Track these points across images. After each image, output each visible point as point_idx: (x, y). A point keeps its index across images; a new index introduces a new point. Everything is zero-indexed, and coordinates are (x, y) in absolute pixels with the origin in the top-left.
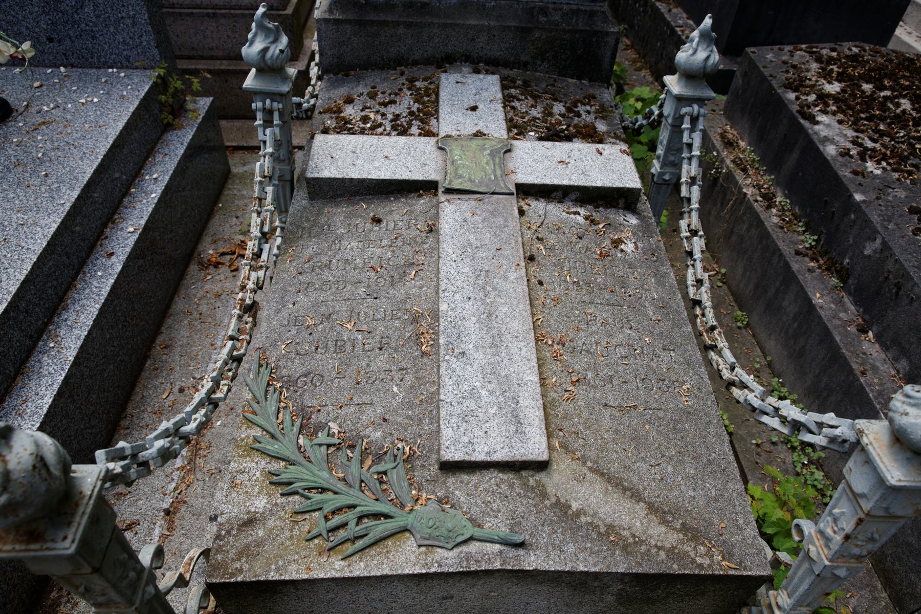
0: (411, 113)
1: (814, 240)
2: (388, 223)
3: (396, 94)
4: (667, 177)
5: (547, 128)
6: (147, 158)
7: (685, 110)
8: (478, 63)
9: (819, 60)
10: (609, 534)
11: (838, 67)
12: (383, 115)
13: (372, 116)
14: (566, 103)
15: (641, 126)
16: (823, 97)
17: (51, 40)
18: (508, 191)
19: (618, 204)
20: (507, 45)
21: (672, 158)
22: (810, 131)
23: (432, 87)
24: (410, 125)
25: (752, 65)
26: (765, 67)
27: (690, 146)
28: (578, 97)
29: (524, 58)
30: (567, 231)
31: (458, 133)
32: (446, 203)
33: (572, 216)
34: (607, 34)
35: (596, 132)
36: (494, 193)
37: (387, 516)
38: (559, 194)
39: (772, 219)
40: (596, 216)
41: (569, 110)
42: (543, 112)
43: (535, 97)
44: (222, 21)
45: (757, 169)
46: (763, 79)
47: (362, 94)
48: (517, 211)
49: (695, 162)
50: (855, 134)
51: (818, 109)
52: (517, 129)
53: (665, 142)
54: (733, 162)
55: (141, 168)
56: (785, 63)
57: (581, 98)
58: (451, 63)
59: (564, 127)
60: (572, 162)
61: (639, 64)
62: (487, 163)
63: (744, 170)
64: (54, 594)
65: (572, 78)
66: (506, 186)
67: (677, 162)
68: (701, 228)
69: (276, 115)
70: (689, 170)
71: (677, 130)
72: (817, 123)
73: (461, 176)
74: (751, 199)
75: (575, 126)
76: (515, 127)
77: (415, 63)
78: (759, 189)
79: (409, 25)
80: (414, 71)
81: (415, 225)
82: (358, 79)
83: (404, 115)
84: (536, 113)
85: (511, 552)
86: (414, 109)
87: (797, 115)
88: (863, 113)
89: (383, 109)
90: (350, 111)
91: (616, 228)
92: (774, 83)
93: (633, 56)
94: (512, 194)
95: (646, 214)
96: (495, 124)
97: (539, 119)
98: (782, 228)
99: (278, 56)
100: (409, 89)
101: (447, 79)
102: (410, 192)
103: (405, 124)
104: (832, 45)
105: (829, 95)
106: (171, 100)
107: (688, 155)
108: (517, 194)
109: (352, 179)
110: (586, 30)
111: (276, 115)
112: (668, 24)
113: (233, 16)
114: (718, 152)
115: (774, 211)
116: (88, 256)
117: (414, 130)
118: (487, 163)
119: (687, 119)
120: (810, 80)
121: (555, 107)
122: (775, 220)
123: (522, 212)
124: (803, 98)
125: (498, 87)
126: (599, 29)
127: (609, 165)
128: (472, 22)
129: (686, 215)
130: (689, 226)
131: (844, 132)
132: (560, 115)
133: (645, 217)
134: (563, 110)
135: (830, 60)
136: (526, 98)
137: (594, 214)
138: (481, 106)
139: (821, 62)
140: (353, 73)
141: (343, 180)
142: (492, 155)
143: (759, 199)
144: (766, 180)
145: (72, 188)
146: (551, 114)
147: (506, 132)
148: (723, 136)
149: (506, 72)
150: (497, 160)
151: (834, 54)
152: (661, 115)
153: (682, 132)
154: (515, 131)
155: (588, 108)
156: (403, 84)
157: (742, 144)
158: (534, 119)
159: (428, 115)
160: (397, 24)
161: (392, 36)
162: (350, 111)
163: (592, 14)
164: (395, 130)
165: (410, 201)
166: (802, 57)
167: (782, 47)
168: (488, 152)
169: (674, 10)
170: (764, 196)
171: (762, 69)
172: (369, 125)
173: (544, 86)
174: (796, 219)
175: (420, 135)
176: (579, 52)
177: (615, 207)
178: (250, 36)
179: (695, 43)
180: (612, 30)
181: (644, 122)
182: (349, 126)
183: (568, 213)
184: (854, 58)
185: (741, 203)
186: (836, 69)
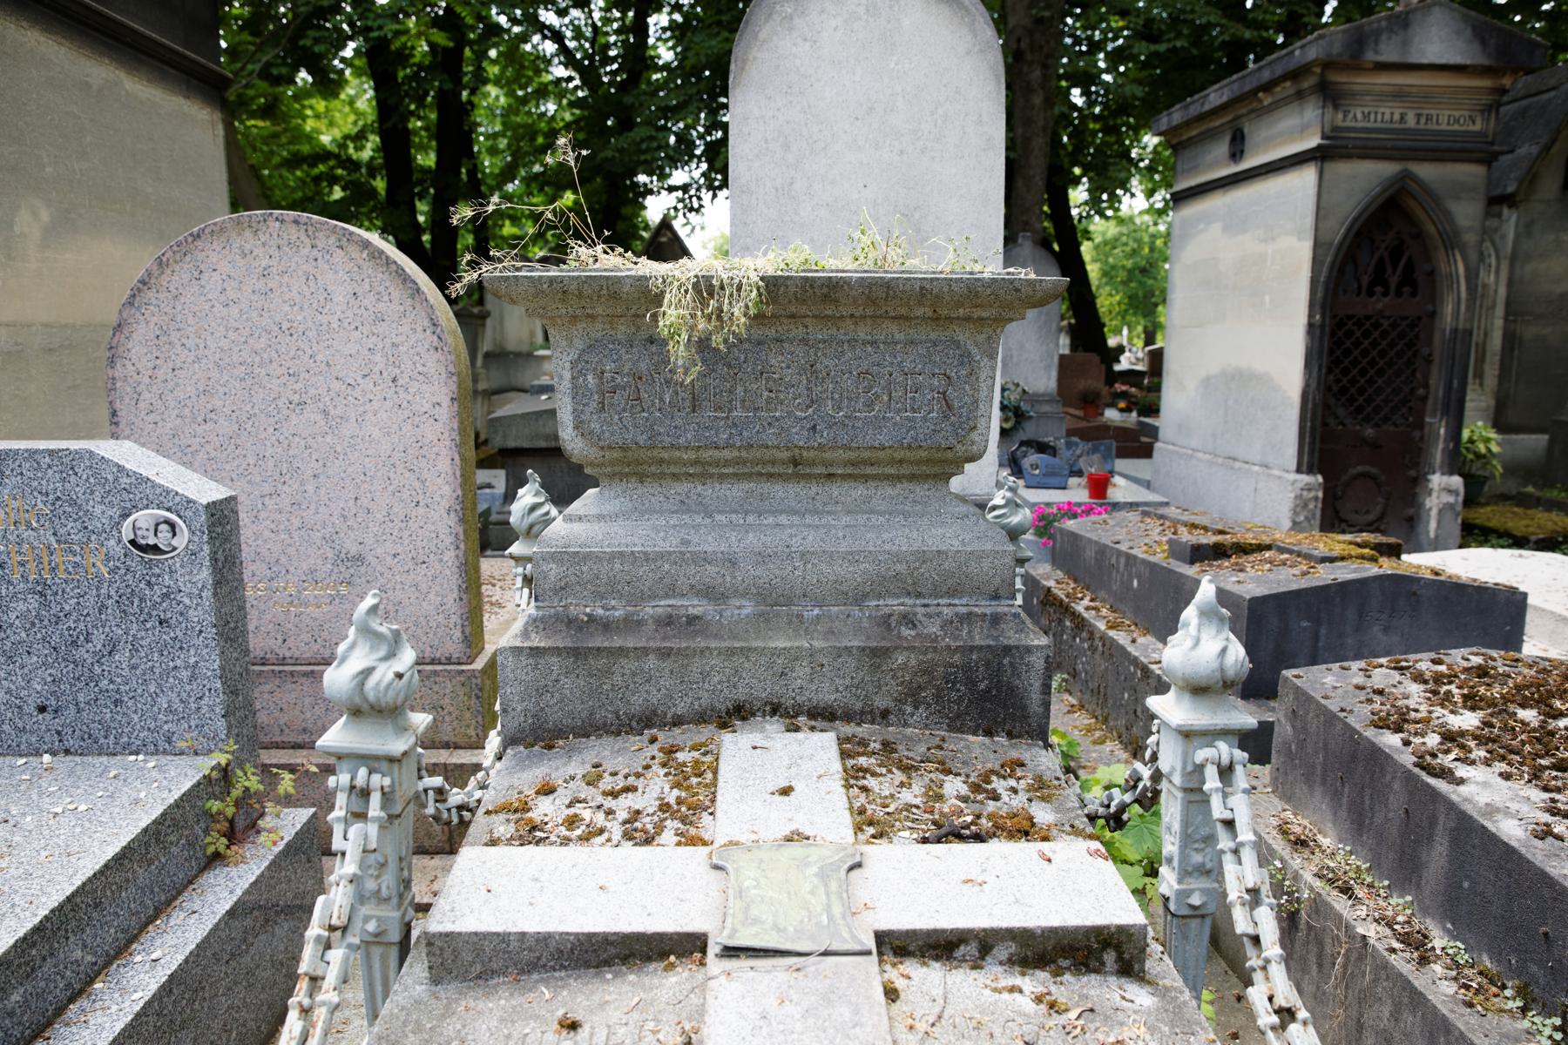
0: (664, 807)
1: (1556, 1029)
3: (638, 775)
4: (1196, 900)
5: (935, 823)
6: (151, 920)
7: (1201, 755)
8: (796, 715)
9: (1419, 678)
11: (1459, 687)
12: (610, 812)
13: (587, 815)
14: (968, 776)
15: (1123, 807)
16: (1451, 737)
17: (42, 709)
18: (858, 948)
19: (1103, 964)
20: (848, 681)
21: (1197, 858)
22: (1454, 797)
23: (708, 759)
24: (660, 828)
25: (1302, 697)
26: (1326, 697)
27: (1229, 824)
28: (989, 766)
29: (881, 702)
30: (997, 1031)
31: (754, 837)
32: (723, 979)
33: (1006, 996)
34: (1029, 650)
35: (1033, 825)
36: (826, 953)
38: (970, 949)
39: (1439, 986)
40: (1059, 993)
41: (976, 788)
42: (926, 794)
43: (907, 769)
45: (1370, 886)
46: (1330, 718)
47: (572, 778)
48: (880, 990)
49: (1248, 856)
50: (1546, 796)
51: (1452, 756)
52: (873, 825)
53: (1176, 827)
54: (1318, 876)
56: (1360, 688)
57: (997, 767)
58: (744, 719)
59: (969, 819)
60: (991, 880)
61: (1098, 734)
62: (812, 893)
63: (1346, 890)
65: (975, 733)
66: (854, 937)
67: (1209, 866)
68: (1299, 1004)
69: (376, 799)
70: (1241, 875)
71: (1195, 794)
72: (1461, 781)
73: (756, 921)
74: (1380, 947)
75: (990, 817)
76: (871, 824)
77: (678, 722)
78: (1389, 925)
79: (665, 654)
80: (676, 735)
81: (654, 1032)
82: (570, 753)
83: (650, 811)
84: (912, 795)
86: (672, 800)
87: (1417, 770)
88: (1542, 757)
89: (609, 803)
90: (545, 809)
91: (1107, 1018)
92: (1351, 720)
93: (1086, 722)
94: (869, 953)
95: (1168, 982)
96: (825, 807)
97: (917, 807)
98: (1470, 1005)
99: (390, 684)
100: (664, 765)
101: (736, 743)
102: (649, 959)
103: (649, 827)
104: (1433, 655)
105: (1462, 733)
107: (1232, 845)
108: (880, 954)
109: (523, 935)
110: (989, 646)
111: (376, 799)
112: (1135, 661)
114: (1282, 860)
115: (1438, 968)
117: (668, 836)
118: (812, 893)
119: (1211, 773)
120: (1416, 711)
121: (947, 785)
122: (1449, 988)
123: (891, 994)
124: (1417, 740)
125: (833, 752)
126: (1011, 642)
128: (781, 643)
129: (1258, 976)
130: (1271, 999)
131: (1522, 793)
132: (959, 798)
133: (1167, 989)
134: (964, 790)
135: (1438, 679)
136: (890, 771)
137: (1053, 988)
138: (799, 787)
139: (1425, 682)
140: (561, 742)
141: (503, 937)
142: (823, 875)
143: (1397, 945)
144: (1399, 905)
146: (940, 798)
147: (851, 832)
148: (1283, 830)
149: (849, 729)
150: (834, 886)
151: (1443, 668)
152: (1157, 776)
153: (1206, 801)
154: (871, 830)
155: (1012, 783)
156: (653, 758)
157: (1325, 842)
158: (909, 807)
159: (697, 808)
160: (645, 651)
161: (634, 674)
162: (545, 809)
163: (996, 620)
164: (630, 839)
165: (647, 980)
166: (1387, 676)
167: (1345, 664)
168: (815, 869)
169: (1141, 640)
170: (1405, 939)
171: (1323, 701)
172: (578, 832)
173: (923, 749)
174: (1492, 982)
175: (679, 844)
176: (982, 686)
177: (1097, 971)
178: (341, 648)
179: (1193, 629)
180: (1036, 642)
181: (1128, 798)
182: (539, 834)
183: (995, 990)
184: (1482, 672)
185: (1361, 958)
186: (1455, 691)
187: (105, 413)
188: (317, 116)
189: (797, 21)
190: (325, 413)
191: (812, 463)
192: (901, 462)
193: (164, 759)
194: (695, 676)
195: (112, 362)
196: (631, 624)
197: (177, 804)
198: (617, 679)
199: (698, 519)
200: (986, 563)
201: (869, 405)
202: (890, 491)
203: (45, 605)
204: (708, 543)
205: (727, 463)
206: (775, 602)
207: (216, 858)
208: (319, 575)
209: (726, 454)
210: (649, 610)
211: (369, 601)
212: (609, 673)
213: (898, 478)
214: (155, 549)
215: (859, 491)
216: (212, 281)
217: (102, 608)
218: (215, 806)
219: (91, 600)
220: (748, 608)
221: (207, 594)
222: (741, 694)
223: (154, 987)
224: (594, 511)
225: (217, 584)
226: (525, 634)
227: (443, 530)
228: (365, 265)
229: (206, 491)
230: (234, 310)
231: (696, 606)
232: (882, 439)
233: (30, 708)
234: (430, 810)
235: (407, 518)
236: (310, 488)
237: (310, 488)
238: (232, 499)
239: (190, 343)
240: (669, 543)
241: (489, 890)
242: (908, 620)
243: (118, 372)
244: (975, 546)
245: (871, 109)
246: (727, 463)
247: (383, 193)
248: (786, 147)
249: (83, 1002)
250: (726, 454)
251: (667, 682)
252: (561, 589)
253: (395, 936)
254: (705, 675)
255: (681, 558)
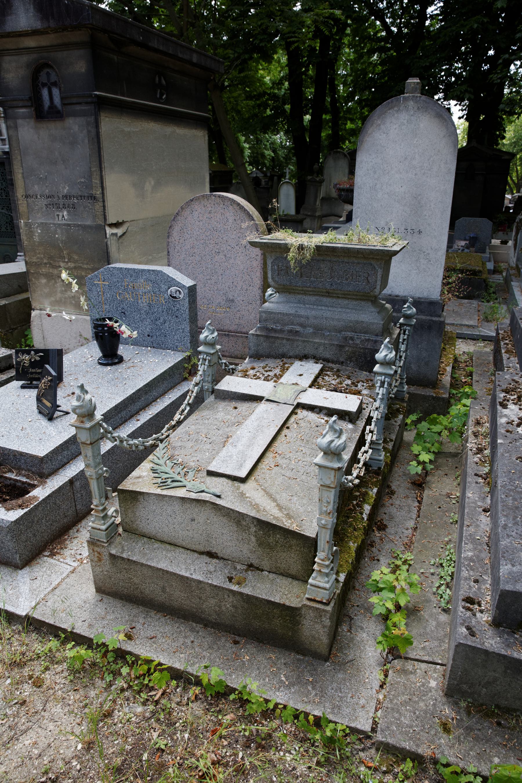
2: (239, 409)
6: (170, 390)
10: (256, 507)
17: (149, 336)
29: (341, 360)
37: (181, 482)
44: (231, 338)
55: (166, 393)
64: (66, 537)
69: (207, 361)
79: (288, 340)
82: (263, 361)
85: (215, 498)
102: (254, 400)
106: (190, 367)
111: (207, 361)
113: (238, 336)
116: (129, 419)
127: (350, 403)
138: (304, 375)
141: (228, 391)
145: (133, 389)
160: (283, 338)
162: (251, 372)
187: (166, 253)
188: (263, 69)
189: (382, 126)
190: (225, 256)
191: (332, 293)
192: (356, 295)
193: (175, 352)
194: (295, 346)
195: (168, 237)
196: (281, 331)
197: (177, 363)
198: (276, 344)
199: (302, 306)
200: (375, 326)
201: (347, 279)
202: (355, 303)
203: (150, 309)
204: (302, 312)
205: (310, 291)
206: (318, 330)
207: (186, 379)
208: (221, 305)
209: (310, 289)
210: (286, 328)
211: (209, 322)
212: (274, 343)
213: (357, 299)
214: (175, 297)
215: (346, 302)
216: (196, 214)
217: (163, 311)
218: (186, 365)
219: (160, 309)
220: (311, 330)
221: (187, 310)
222: (306, 352)
223: (169, 402)
224: (276, 301)
225: (190, 308)
226: (256, 331)
227: (257, 294)
228: (238, 211)
229: (188, 282)
230: (201, 223)
231: (298, 328)
232: (350, 289)
233: (146, 335)
234: (223, 368)
235: (247, 290)
236: (220, 278)
237: (220, 278)
238: (195, 285)
239: (189, 232)
240: (292, 311)
241: (230, 383)
242: (352, 339)
243: (170, 240)
244: (372, 321)
245: (406, 158)
246: (310, 291)
247: (289, 111)
248: (375, 172)
249: (155, 403)
250: (310, 289)
251: (288, 347)
252: (266, 320)
253: (211, 390)
254: (297, 346)
255: (295, 316)
